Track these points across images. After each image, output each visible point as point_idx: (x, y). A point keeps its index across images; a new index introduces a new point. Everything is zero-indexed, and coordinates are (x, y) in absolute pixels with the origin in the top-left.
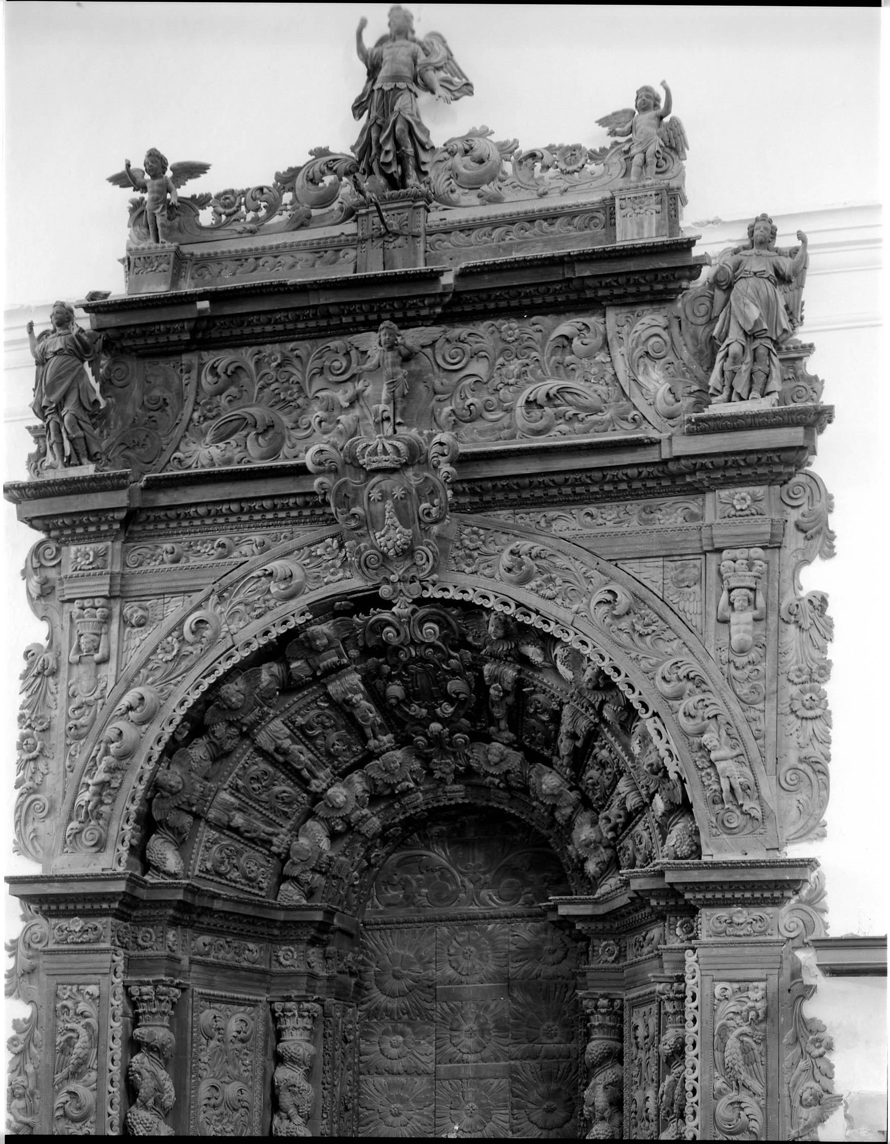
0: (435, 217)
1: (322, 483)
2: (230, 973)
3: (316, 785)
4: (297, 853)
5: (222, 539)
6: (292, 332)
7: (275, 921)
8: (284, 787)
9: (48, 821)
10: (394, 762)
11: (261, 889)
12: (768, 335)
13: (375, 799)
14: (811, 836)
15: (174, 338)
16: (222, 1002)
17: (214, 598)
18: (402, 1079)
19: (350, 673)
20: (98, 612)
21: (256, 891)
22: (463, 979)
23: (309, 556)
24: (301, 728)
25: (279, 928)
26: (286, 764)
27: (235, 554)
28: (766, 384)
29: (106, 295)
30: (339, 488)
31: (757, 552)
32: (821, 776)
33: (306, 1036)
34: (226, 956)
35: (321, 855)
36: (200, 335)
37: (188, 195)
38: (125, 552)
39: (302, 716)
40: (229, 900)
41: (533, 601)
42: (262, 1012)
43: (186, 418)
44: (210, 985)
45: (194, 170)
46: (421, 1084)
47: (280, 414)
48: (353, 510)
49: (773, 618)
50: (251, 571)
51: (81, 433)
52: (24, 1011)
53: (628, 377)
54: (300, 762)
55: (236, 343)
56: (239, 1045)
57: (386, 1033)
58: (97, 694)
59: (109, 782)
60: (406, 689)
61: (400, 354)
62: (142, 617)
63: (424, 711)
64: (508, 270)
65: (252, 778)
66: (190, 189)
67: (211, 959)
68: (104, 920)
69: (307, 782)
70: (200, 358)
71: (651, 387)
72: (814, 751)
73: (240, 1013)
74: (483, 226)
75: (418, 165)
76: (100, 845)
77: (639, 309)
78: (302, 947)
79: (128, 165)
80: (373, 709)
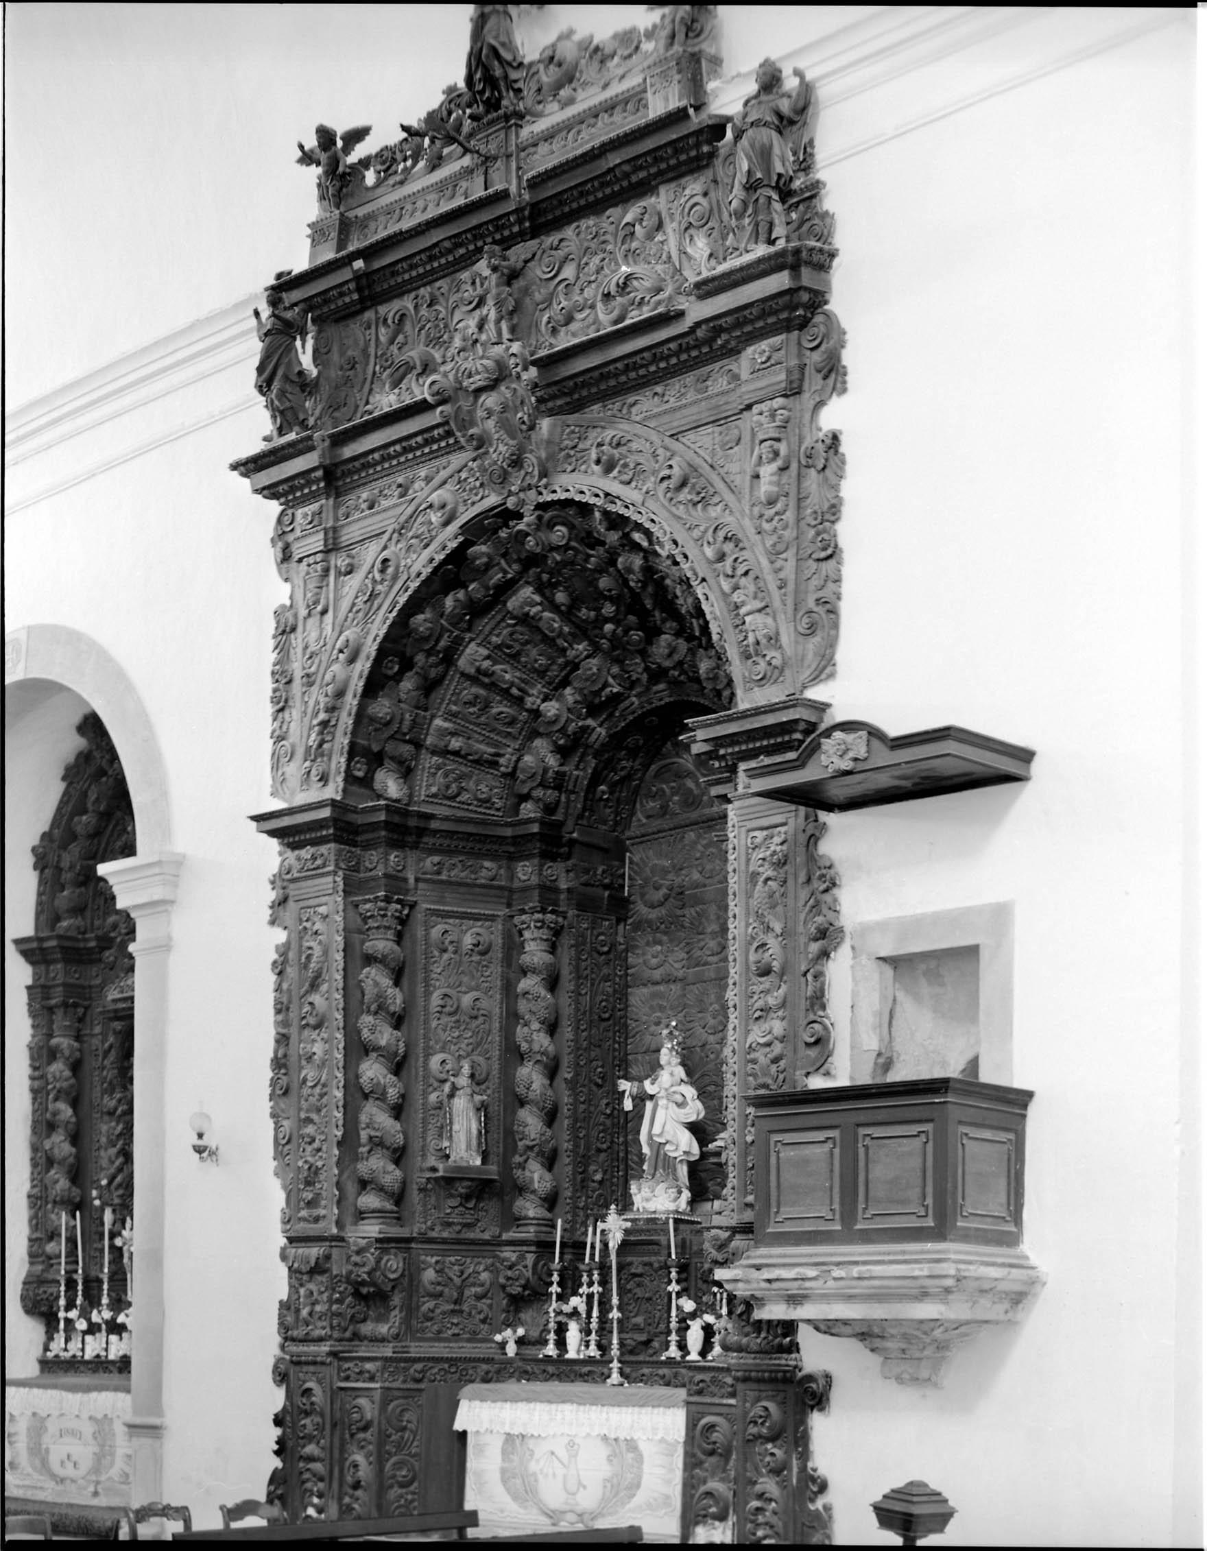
0: (525, 133)
1: (442, 412)
2: (462, 890)
3: (529, 702)
4: (523, 771)
5: (400, 480)
6: (433, 271)
7: (506, 838)
8: (500, 708)
9: (291, 764)
10: (590, 669)
11: (498, 810)
12: (765, 183)
13: (593, 711)
14: (823, 676)
15: (347, 300)
16: (457, 918)
17: (396, 535)
18: (662, 988)
19: (522, 587)
20: (319, 567)
21: (492, 812)
22: (707, 881)
23: (459, 482)
24: (498, 647)
25: (513, 845)
26: (493, 684)
27: (410, 492)
28: (770, 231)
29: (290, 273)
30: (456, 412)
31: (780, 401)
32: (832, 616)
33: (544, 946)
34: (458, 874)
35: (546, 770)
36: (366, 293)
37: (356, 161)
38: (336, 507)
39: (498, 636)
40: (446, 819)
41: (615, 488)
42: (499, 926)
43: (370, 371)
44: (441, 901)
45: (358, 135)
46: (675, 988)
47: (432, 351)
48: (471, 431)
49: (794, 466)
50: (420, 505)
51: (288, 404)
52: (281, 936)
53: (676, 251)
54: (505, 682)
55: (399, 292)
56: (476, 958)
57: (648, 944)
58: (322, 643)
59: (329, 721)
60: (570, 595)
61: (503, 274)
62: (349, 565)
63: (593, 614)
64: (564, 172)
65: (465, 703)
66: (360, 151)
67: (444, 877)
68: (329, 846)
69: (869, 733)
70: (377, 312)
71: (697, 256)
72: (826, 594)
73: (478, 927)
74: (560, 131)
75: (510, 84)
76: (324, 779)
77: (683, 181)
78: (536, 861)
79: (301, 147)
80: (557, 619)
